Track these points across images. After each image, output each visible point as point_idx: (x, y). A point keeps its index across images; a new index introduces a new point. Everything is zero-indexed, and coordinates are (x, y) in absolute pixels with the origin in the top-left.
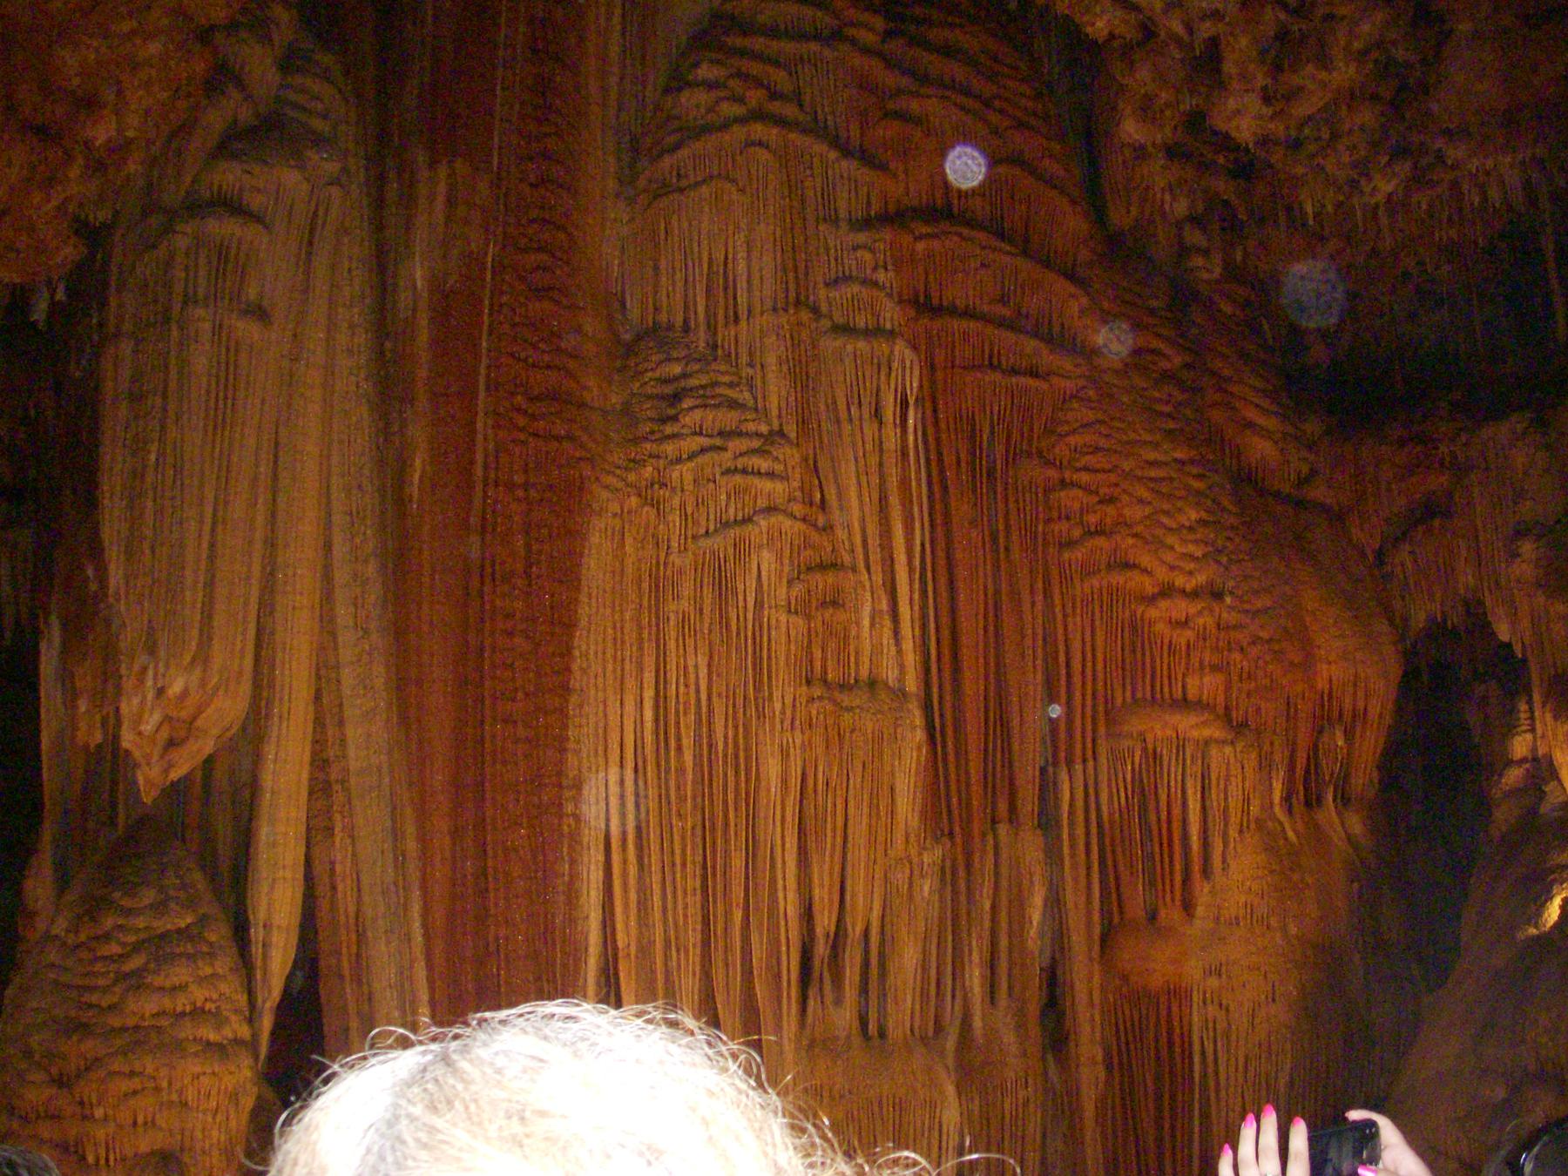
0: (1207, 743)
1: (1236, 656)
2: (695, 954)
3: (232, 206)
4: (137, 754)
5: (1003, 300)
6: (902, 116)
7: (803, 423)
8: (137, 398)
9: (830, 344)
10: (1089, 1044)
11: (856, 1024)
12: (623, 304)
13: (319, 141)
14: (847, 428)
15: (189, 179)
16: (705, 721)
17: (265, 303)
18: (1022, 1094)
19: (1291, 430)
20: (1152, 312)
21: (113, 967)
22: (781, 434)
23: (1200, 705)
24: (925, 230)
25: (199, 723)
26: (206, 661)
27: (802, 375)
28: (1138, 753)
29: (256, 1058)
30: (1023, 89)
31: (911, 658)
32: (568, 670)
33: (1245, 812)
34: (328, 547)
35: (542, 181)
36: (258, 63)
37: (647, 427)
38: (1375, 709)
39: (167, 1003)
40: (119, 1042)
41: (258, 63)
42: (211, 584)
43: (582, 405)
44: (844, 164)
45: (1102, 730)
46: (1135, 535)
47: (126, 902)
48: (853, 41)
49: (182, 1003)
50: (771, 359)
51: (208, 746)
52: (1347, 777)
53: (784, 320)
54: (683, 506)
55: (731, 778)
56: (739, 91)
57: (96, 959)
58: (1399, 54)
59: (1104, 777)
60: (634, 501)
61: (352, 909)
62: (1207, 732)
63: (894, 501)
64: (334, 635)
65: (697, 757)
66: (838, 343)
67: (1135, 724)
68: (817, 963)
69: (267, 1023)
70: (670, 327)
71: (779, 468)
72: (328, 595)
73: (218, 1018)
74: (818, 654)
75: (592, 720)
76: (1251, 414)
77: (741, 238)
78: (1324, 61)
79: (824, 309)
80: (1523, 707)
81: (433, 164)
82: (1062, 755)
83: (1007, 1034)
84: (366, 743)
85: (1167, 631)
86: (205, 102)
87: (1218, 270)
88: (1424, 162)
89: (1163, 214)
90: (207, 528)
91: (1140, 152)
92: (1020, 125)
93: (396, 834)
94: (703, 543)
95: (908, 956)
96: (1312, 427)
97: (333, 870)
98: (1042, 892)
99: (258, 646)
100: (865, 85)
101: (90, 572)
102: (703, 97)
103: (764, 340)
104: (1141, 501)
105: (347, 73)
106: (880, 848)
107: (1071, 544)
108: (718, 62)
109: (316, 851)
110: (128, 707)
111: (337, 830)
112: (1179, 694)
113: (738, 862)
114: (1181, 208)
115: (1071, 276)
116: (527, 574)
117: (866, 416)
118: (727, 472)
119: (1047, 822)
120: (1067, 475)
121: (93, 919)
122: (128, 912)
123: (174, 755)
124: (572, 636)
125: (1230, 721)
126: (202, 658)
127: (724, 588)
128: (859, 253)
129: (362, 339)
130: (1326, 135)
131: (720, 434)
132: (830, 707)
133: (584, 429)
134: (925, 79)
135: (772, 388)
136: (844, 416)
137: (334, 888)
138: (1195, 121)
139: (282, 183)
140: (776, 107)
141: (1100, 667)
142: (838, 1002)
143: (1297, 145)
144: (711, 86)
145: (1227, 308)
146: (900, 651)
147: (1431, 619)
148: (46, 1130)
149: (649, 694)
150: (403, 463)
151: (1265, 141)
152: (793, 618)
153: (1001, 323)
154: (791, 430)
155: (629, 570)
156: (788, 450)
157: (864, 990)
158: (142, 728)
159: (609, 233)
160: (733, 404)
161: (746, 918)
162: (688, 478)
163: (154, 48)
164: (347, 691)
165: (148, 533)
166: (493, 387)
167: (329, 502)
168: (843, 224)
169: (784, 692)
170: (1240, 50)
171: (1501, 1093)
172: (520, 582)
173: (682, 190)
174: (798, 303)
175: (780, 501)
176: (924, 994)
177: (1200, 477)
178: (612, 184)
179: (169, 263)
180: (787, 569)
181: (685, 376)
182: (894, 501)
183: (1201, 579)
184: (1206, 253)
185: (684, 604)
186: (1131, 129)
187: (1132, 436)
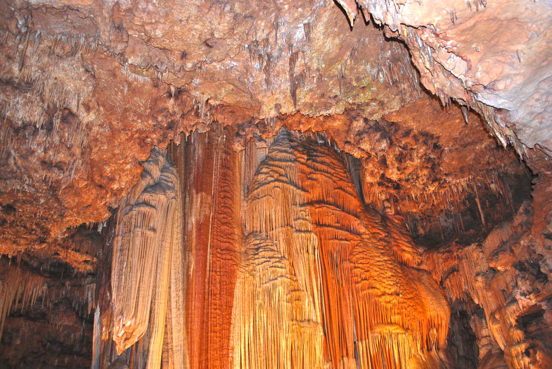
0: (398, 334)
1: (404, 310)
3: (146, 203)
4: (117, 342)
5: (338, 222)
6: (311, 179)
7: (289, 254)
8: (121, 250)
9: (295, 234)
12: (245, 226)
13: (169, 188)
14: (300, 255)
15: (137, 197)
16: (266, 331)
17: (155, 228)
19: (415, 251)
22: (284, 257)
24: (318, 206)
25: (134, 333)
26: (136, 317)
27: (289, 243)
30: (341, 170)
31: (319, 314)
32: (231, 318)
33: (410, 352)
34: (170, 288)
35: (225, 197)
36: (156, 172)
37: (251, 256)
38: (444, 323)
41: (156, 172)
42: (138, 297)
44: (298, 191)
46: (375, 280)
48: (299, 162)
52: (438, 343)
53: (284, 229)
54: (260, 275)
55: (273, 345)
58: (432, 156)
59: (371, 344)
60: (248, 275)
62: (398, 331)
63: (313, 272)
64: (171, 310)
65: (264, 341)
67: (378, 329)
70: (256, 232)
71: (283, 265)
74: (294, 313)
75: (237, 331)
76: (404, 248)
77: (273, 210)
78: (412, 159)
79: (294, 226)
80: (484, 321)
81: (197, 193)
82: (359, 338)
85: (385, 305)
86: (141, 179)
87: (393, 212)
88: (441, 182)
89: (379, 200)
90: (138, 283)
91: (372, 184)
92: (341, 179)
94: (265, 285)
96: (421, 250)
99: (151, 312)
100: (303, 172)
101: (108, 295)
102: (263, 176)
103: (279, 233)
104: (376, 271)
106: (313, 365)
111: (170, 362)
112: (389, 321)
114: (383, 197)
115: (356, 216)
117: (305, 252)
119: (356, 356)
120: (356, 265)
123: (127, 342)
124: (231, 310)
125: (404, 328)
126: (135, 315)
127: (270, 296)
128: (302, 212)
130: (415, 177)
131: (269, 258)
133: (235, 257)
134: (317, 170)
135: (281, 246)
136: (299, 252)
138: (383, 176)
139: (160, 198)
140: (281, 178)
141: (368, 314)
143: (407, 180)
144: (266, 173)
145: (396, 221)
147: (457, 299)
149: (252, 324)
150: (189, 267)
151: (400, 180)
152: (288, 304)
154: (286, 256)
155: (246, 292)
156: (285, 261)
159: (242, 209)
160: (272, 250)
162: (261, 269)
163: (128, 166)
164: (173, 325)
166: (212, 247)
168: (298, 205)
170: (390, 158)
172: (218, 296)
173: (258, 199)
174: (287, 225)
175: (284, 274)
177: (391, 264)
178: (242, 197)
179: (131, 218)
180: (286, 291)
181: (260, 243)
182: (313, 272)
183: (393, 290)
184: (390, 208)
186: (369, 179)
187: (373, 255)
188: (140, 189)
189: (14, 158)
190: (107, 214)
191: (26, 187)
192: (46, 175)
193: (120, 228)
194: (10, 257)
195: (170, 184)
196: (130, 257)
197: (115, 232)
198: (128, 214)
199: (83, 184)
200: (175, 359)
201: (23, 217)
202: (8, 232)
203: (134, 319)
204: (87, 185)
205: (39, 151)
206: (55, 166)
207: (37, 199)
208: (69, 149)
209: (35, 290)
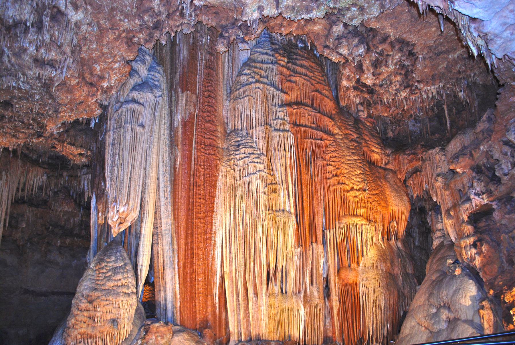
0: (362, 225)
1: (369, 204)
2: (242, 273)
3: (135, 101)
4: (112, 226)
5: (314, 123)
7: (268, 151)
8: (113, 145)
9: (274, 133)
10: (335, 297)
11: (280, 290)
12: (228, 124)
13: (156, 87)
14: (277, 152)
16: (245, 219)
17: (144, 124)
18: (319, 308)
19: (383, 152)
20: (350, 125)
21: (104, 275)
22: (263, 153)
23: (361, 216)
24: (296, 107)
25: (127, 218)
26: (129, 204)
27: (267, 141)
28: (345, 227)
29: (138, 298)
30: (320, 74)
31: (292, 205)
33: (372, 240)
34: (158, 179)
35: (209, 96)
36: (143, 71)
38: (404, 217)
39: (116, 283)
40: (104, 293)
41: (143, 71)
42: (130, 187)
43: (217, 147)
45: (337, 222)
46: (345, 176)
47: (108, 260)
48: (280, 64)
49: (120, 283)
50: (260, 137)
51: (129, 224)
52: (397, 234)
53: (263, 128)
56: (254, 76)
57: (100, 273)
58: (406, 63)
60: (229, 169)
61: (162, 262)
62: (362, 222)
63: (288, 168)
66: (276, 133)
67: (344, 220)
68: (271, 276)
69: (141, 289)
70: (238, 130)
71: (262, 161)
72: (158, 190)
73: (128, 287)
74: (271, 204)
75: (219, 218)
77: (254, 110)
78: (387, 66)
79: (273, 125)
80: (440, 217)
81: (182, 92)
83: (316, 292)
84: (166, 222)
87: (366, 115)
88: (413, 88)
89: (353, 103)
90: (129, 174)
91: (347, 88)
92: (318, 83)
93: (172, 244)
94: (244, 178)
95: (292, 274)
96: (389, 151)
97: (158, 253)
98: (324, 260)
100: (283, 74)
101: (103, 184)
102: (245, 77)
103: (259, 131)
104: (346, 169)
105: (164, 72)
106: (285, 249)
107: (329, 178)
108: (249, 69)
109: (154, 249)
110: (110, 215)
111: (159, 243)
112: (355, 213)
113: (252, 251)
114: (358, 101)
115: (330, 118)
116: (204, 185)
118: (250, 162)
119: (324, 243)
121: (100, 264)
122: (108, 262)
123: (121, 226)
124: (214, 199)
127: (249, 189)
129: (167, 131)
130: (388, 83)
131: (249, 154)
132: (273, 215)
134: (297, 73)
135: (261, 143)
137: (158, 257)
138: (358, 81)
139: (148, 96)
140: (262, 79)
141: (336, 207)
142: (276, 285)
144: (247, 75)
145: (368, 124)
146: (290, 203)
148: (86, 314)
149: (232, 212)
150: (175, 161)
151: (374, 85)
153: (313, 128)
154: (265, 153)
156: (264, 157)
157: (282, 282)
158: (114, 219)
159: (224, 108)
160: (252, 147)
161: (254, 264)
162: (241, 164)
163: (117, 65)
164: (162, 212)
165: (116, 175)
166: (197, 143)
167: (159, 168)
168: (277, 106)
169: (263, 212)
170: (367, 64)
171: (434, 310)
173: (240, 99)
174: (267, 124)
176: (296, 283)
178: (225, 97)
179: (121, 115)
181: (241, 141)
182: (288, 168)
183: (360, 186)
184: (363, 111)
185: (240, 192)
186: (345, 83)
187: (344, 154)
188: (129, 87)
189: (8, 56)
190: (99, 111)
191: (21, 84)
192: (39, 73)
193: (111, 124)
194: (10, 150)
195: (157, 83)
196: (121, 151)
197: (106, 128)
198: (118, 110)
199: (75, 82)
200: (164, 241)
201: (21, 113)
202: (7, 127)
203: (127, 206)
204: (78, 83)
205: (31, 49)
206: (48, 64)
207: (32, 96)
208: (60, 47)
209: (36, 180)
